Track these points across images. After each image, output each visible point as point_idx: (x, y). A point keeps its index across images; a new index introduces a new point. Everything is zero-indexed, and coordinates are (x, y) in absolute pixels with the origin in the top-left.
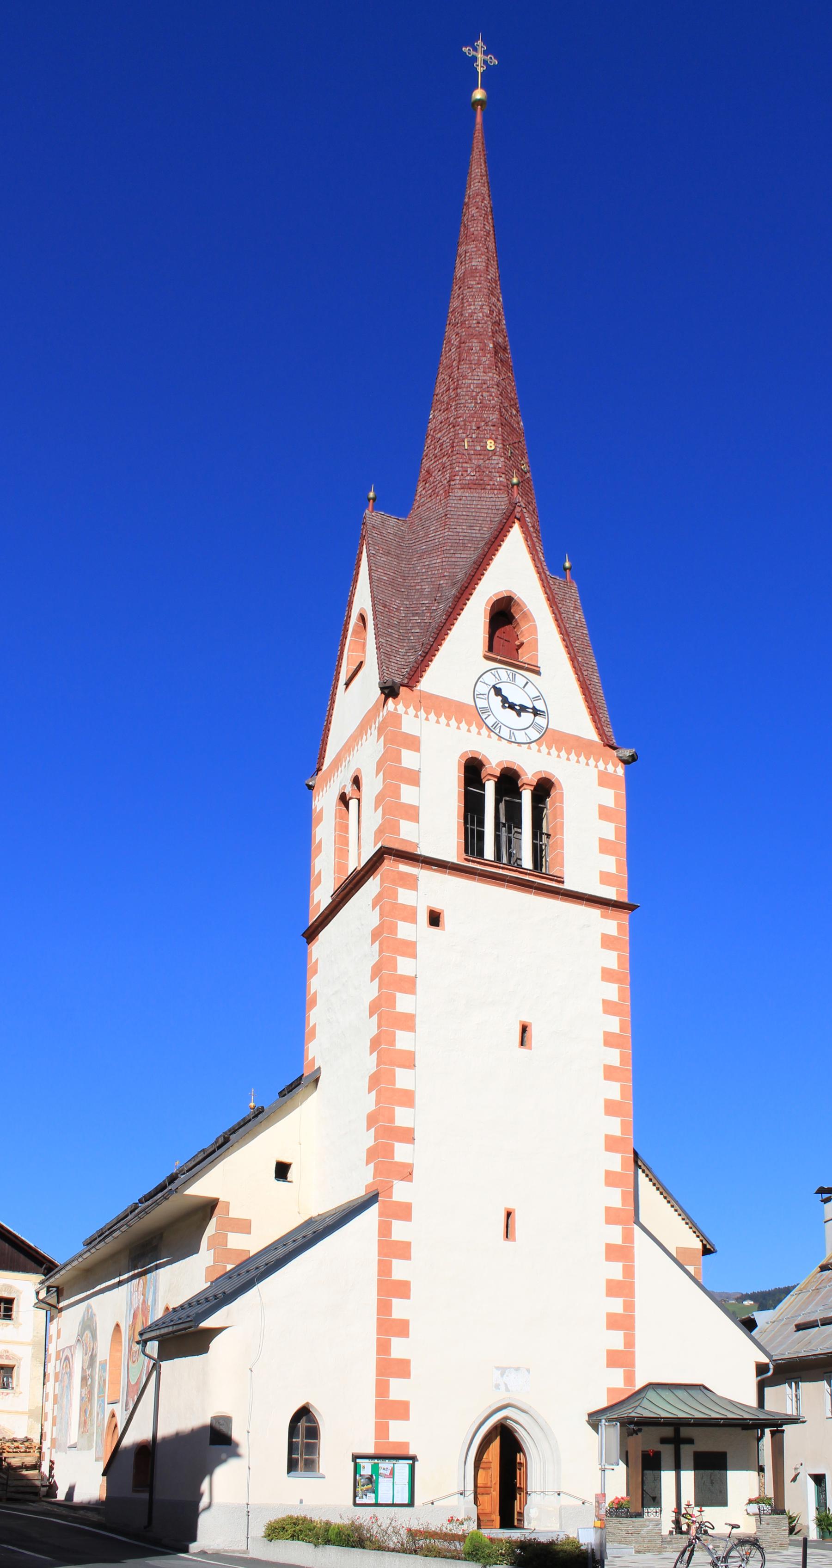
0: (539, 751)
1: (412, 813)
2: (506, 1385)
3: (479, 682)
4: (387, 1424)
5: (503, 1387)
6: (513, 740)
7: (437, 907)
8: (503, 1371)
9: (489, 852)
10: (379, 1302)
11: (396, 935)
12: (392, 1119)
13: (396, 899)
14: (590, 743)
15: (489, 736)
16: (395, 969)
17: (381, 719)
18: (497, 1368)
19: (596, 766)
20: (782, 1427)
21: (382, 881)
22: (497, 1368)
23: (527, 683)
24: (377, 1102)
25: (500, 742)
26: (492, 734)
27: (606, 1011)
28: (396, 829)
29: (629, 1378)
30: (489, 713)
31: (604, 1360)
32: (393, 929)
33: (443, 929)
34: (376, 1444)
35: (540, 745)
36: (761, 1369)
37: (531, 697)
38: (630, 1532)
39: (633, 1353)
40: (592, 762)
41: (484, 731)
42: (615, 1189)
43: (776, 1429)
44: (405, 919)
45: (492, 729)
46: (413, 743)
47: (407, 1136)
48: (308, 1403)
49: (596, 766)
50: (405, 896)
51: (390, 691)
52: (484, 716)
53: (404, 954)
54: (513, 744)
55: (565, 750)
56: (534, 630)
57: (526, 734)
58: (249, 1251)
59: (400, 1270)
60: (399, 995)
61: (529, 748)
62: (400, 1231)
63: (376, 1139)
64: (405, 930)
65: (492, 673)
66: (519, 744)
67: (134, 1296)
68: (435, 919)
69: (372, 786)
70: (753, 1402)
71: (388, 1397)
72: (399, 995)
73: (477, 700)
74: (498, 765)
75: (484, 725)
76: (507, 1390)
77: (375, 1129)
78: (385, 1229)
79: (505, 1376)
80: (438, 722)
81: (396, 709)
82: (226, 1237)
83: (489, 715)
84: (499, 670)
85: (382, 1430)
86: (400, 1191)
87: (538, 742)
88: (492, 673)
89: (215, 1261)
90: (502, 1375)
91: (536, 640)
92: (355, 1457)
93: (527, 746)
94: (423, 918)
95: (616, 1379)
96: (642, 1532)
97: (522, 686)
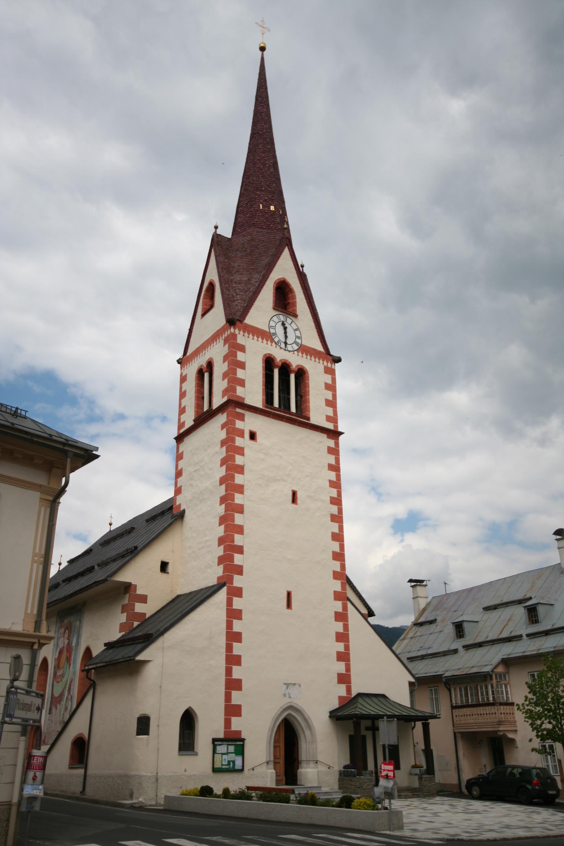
0: (298, 355)
1: (242, 383)
2: (289, 694)
3: (271, 321)
4: (230, 719)
5: (287, 695)
6: (286, 349)
7: (254, 430)
8: (287, 685)
9: (276, 404)
10: (227, 644)
11: (235, 444)
12: (233, 541)
13: (235, 425)
14: (320, 352)
15: (276, 347)
16: (234, 461)
17: (226, 335)
18: (285, 684)
19: (323, 364)
20: (428, 721)
21: (228, 416)
22: (285, 684)
23: (292, 322)
24: (225, 531)
25: (281, 350)
26: (277, 346)
27: (331, 486)
28: (235, 390)
29: (349, 690)
30: (276, 336)
31: (336, 680)
32: (233, 441)
33: (256, 442)
34: (225, 732)
35: (298, 352)
36: (411, 684)
37: (294, 329)
38: (357, 786)
39: (350, 675)
40: (321, 361)
41: (274, 344)
42: (338, 581)
43: (424, 722)
44: (239, 436)
45: (277, 343)
46: (242, 349)
47: (240, 550)
48: (190, 707)
49: (323, 364)
50: (239, 424)
51: (231, 322)
52: (273, 337)
53: (238, 454)
54: (287, 351)
55: (309, 355)
56: (294, 297)
57: (292, 347)
58: (145, 614)
59: (237, 626)
60: (236, 475)
61: (294, 353)
62: (237, 603)
63: (224, 551)
64: (239, 442)
65: (277, 316)
66: (289, 351)
67: (61, 640)
68: (253, 436)
69: (220, 368)
70: (407, 704)
71: (231, 703)
72: (236, 475)
73: (270, 329)
74: (281, 360)
75: (274, 342)
76: (290, 697)
77: (224, 546)
78: (229, 602)
79: (288, 689)
80: (253, 339)
81: (235, 332)
82: (134, 605)
83: (276, 337)
84: (280, 315)
85: (228, 723)
86: (238, 581)
87: (298, 350)
88: (277, 316)
89: (127, 620)
90: (287, 688)
91: (296, 302)
92: (214, 740)
93: (293, 352)
94: (247, 435)
95: (342, 690)
96: (364, 787)
97: (290, 323)
